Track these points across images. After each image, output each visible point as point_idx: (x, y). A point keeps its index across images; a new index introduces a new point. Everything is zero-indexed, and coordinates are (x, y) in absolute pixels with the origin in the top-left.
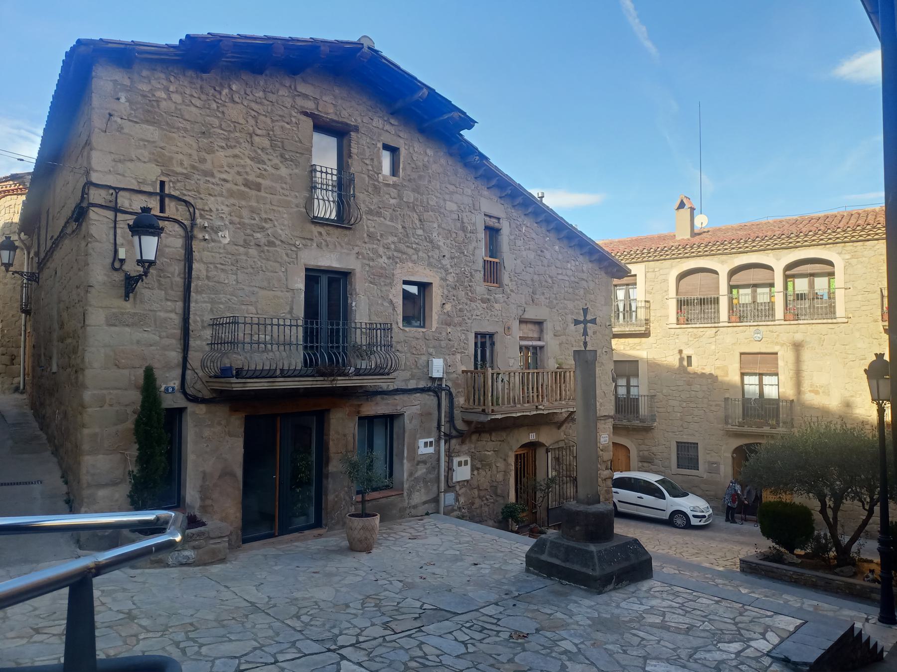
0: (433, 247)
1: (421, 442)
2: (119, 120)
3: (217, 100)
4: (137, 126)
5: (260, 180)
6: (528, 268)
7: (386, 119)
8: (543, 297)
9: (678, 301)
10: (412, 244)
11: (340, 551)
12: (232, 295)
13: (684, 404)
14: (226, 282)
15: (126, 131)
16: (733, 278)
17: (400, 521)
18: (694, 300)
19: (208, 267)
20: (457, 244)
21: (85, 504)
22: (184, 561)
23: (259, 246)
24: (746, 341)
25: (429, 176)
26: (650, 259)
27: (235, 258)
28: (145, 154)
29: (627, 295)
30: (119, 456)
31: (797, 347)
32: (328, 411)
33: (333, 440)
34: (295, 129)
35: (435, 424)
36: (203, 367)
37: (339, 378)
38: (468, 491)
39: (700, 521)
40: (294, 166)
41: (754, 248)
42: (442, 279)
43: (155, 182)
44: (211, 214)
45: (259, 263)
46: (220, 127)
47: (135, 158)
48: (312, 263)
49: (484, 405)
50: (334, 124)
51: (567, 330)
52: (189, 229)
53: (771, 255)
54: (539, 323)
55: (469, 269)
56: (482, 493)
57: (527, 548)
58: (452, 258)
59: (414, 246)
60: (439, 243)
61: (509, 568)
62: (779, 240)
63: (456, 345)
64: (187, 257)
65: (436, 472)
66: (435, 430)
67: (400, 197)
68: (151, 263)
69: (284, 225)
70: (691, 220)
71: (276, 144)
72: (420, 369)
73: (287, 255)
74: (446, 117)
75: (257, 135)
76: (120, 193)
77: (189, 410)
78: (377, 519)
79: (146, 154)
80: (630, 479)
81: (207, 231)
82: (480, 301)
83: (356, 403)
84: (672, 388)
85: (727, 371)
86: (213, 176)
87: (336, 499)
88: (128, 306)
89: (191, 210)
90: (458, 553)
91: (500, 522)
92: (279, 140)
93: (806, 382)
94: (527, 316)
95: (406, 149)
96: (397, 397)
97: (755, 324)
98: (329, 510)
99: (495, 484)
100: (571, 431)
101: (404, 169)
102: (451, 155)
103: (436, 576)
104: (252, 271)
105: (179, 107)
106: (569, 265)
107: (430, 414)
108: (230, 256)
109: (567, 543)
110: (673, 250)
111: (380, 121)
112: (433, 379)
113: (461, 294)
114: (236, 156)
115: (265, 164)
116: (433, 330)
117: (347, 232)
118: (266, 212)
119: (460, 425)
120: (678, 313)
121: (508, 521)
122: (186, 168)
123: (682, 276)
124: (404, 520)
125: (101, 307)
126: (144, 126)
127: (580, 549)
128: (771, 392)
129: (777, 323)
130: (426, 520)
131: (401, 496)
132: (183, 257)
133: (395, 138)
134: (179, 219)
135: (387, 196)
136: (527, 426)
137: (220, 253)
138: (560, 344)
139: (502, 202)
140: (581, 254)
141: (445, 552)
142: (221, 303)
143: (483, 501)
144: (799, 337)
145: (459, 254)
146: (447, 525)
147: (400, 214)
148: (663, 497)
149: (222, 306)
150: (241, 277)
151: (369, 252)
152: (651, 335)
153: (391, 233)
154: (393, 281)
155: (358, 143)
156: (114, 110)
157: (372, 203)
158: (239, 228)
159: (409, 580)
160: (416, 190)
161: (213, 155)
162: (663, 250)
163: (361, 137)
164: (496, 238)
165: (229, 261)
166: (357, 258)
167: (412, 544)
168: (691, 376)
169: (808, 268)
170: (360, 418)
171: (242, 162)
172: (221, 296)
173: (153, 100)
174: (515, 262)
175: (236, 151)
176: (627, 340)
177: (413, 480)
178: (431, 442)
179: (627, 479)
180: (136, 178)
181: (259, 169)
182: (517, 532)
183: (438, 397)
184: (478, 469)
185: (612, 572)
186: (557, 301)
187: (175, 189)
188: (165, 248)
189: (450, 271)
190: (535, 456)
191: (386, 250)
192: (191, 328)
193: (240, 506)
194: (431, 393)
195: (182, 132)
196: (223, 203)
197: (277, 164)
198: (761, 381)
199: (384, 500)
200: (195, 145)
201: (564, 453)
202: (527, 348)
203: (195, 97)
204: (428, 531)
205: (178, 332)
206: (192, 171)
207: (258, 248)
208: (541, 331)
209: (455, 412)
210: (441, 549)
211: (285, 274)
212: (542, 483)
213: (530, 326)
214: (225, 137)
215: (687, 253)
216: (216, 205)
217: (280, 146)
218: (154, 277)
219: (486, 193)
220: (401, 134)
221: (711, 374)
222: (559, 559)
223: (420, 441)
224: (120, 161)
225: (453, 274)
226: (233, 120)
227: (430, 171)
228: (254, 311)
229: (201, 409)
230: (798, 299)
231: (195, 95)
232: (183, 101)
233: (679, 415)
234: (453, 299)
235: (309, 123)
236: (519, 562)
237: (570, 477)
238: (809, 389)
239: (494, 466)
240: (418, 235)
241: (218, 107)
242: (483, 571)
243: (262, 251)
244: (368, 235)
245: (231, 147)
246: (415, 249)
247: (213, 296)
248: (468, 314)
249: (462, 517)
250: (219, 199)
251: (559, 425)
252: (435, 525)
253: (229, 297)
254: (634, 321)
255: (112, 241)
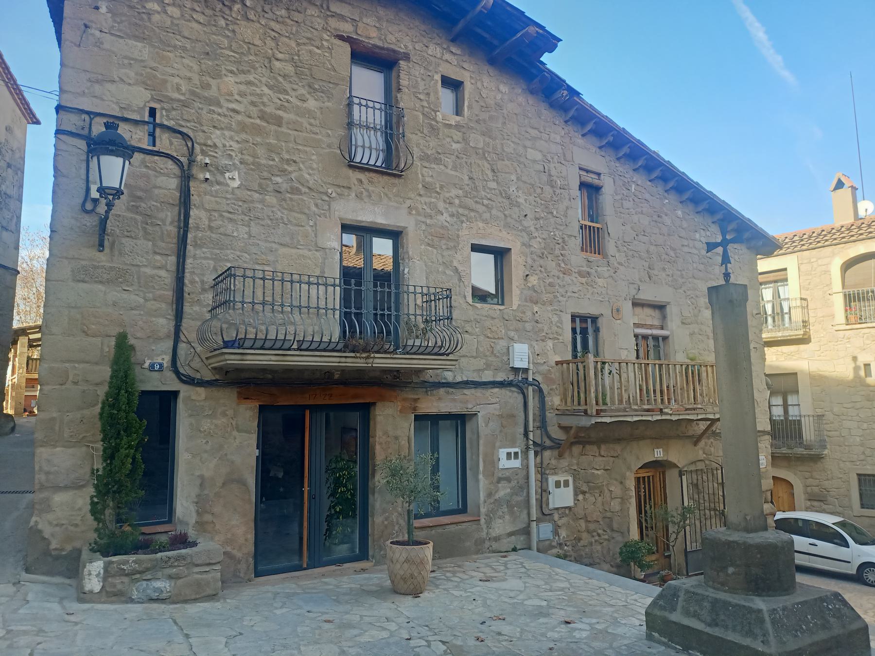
0: (510, 204)
1: (503, 453)
2: (97, 33)
3: (226, 17)
4: (121, 41)
5: (280, 113)
6: (640, 237)
7: (445, 46)
8: (664, 275)
9: (845, 295)
10: (482, 199)
11: (380, 593)
12: (242, 251)
13: (865, 426)
14: (235, 234)
15: (106, 46)
17: (476, 556)
19: (211, 215)
20: (543, 202)
21: (36, 512)
22: (155, 595)
25: (503, 117)
26: (804, 247)
27: (246, 206)
28: (131, 74)
29: (776, 294)
30: (84, 449)
32: (374, 404)
33: (381, 444)
34: (326, 54)
35: (521, 430)
36: (202, 340)
37: (377, 355)
38: (571, 522)
40: (326, 99)
42: (523, 244)
43: (143, 108)
44: (216, 150)
45: (279, 213)
46: (230, 48)
47: (117, 79)
48: (350, 217)
49: (586, 405)
50: (377, 50)
51: (699, 318)
52: (186, 168)
54: (661, 308)
55: (561, 234)
56: (592, 526)
57: (649, 600)
58: (537, 219)
59: (486, 202)
60: (519, 200)
61: (620, 631)
63: (546, 328)
64: (182, 200)
65: (525, 494)
66: (520, 437)
67: (465, 140)
68: (118, 193)
69: (313, 169)
70: (853, 202)
71: (302, 72)
73: (316, 205)
75: (277, 60)
76: (95, 119)
77: (181, 396)
78: (428, 551)
79: (132, 74)
80: (796, 520)
81: (209, 171)
82: (577, 275)
84: (845, 405)
86: (219, 105)
87: (386, 523)
88: (102, 258)
89: (190, 144)
90: (544, 603)
91: (618, 566)
92: (306, 66)
94: (643, 296)
95: (472, 84)
96: (466, 391)
98: (376, 537)
99: (608, 514)
100: (712, 449)
101: (470, 107)
102: (532, 92)
103: (501, 638)
104: (269, 222)
105: (176, 22)
106: (697, 236)
107: (512, 416)
108: (240, 203)
109: (714, 595)
110: (834, 234)
111: (438, 49)
112: (516, 370)
113: (551, 264)
114: (249, 83)
115: (288, 94)
116: (515, 307)
117: (396, 181)
118: (288, 152)
119: (556, 433)
120: (846, 310)
121: (629, 565)
122: (183, 94)
123: (848, 265)
124: (480, 556)
125: (67, 258)
126: (131, 42)
127: (737, 605)
130: (512, 556)
131: (476, 522)
132: (178, 202)
133: (458, 70)
134: (175, 154)
135: (448, 140)
136: (650, 438)
137: (227, 199)
138: (692, 334)
139: (603, 153)
140: (713, 222)
141: (525, 602)
143: (593, 536)
145: (546, 214)
146: (539, 565)
147: (466, 163)
148: (847, 545)
150: (255, 229)
151: (425, 207)
152: (812, 340)
153: (455, 184)
154: (459, 244)
155: (409, 74)
156: (92, 21)
157: (428, 147)
158: (252, 169)
159: (459, 642)
160: (487, 133)
161: (219, 80)
162: (820, 235)
163: (413, 66)
164: (596, 198)
165: (240, 209)
166: (410, 213)
167: (481, 587)
170: (418, 418)
171: (258, 91)
173: (144, 13)
174: (623, 228)
175: (251, 78)
176: (780, 348)
177: (494, 503)
178: (516, 454)
179: (792, 521)
180: (117, 103)
182: (643, 581)
183: (523, 394)
184: (584, 493)
185: (799, 649)
186: (683, 280)
187: (169, 119)
188: (153, 189)
189: (534, 235)
190: (664, 481)
191: (447, 206)
192: (186, 289)
193: (252, 525)
194: (514, 389)
195: (180, 51)
196: (231, 138)
197: (304, 95)
199: (452, 528)
200: (196, 68)
201: (705, 478)
202: (645, 337)
203: (197, 11)
204: (509, 572)
205: (169, 294)
206: (192, 98)
207: (279, 195)
208: (664, 317)
209: (548, 414)
210: (521, 597)
211: (314, 229)
212: (675, 514)
213: (648, 311)
214: (235, 60)
215: (852, 236)
216: (223, 140)
217: (308, 74)
218: (139, 224)
219: (580, 141)
220: (466, 65)
222: (702, 621)
223: (501, 450)
224: (97, 81)
225: (538, 239)
226: (246, 40)
227: (505, 111)
229: (201, 393)
231: (198, 9)
232: (183, 16)
233: (858, 439)
234: (540, 271)
235: (347, 49)
236: (637, 623)
237: (715, 510)
239: (606, 491)
240: (491, 189)
241: (227, 25)
242: (577, 634)
244: (423, 186)
245: (243, 72)
246: (487, 206)
248: (561, 290)
249: (565, 557)
250: (227, 133)
251: (696, 440)
252: (522, 563)
254: (787, 325)
255: (84, 177)
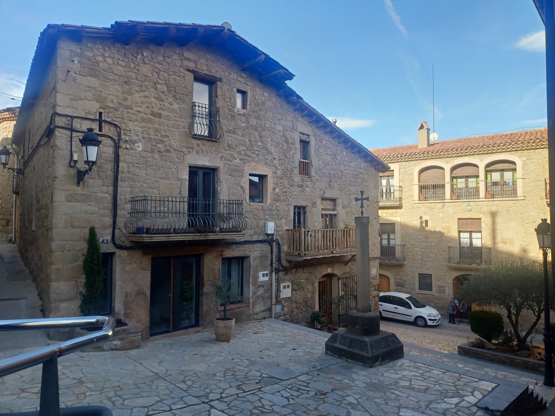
0: (268, 153)
1: (261, 274)
2: (74, 74)
3: (134, 62)
4: (85, 78)
5: (161, 112)
6: (327, 166)
7: (239, 73)
8: (336, 184)
9: (419, 186)
10: (255, 151)
11: (211, 341)
12: (144, 182)
13: (423, 250)
14: (140, 174)
15: (78, 81)
16: (453, 172)
17: (248, 322)
18: (429, 185)
19: (129, 165)
20: (283, 151)
21: (52, 312)
22: (114, 347)
23: (160, 152)
24: (462, 211)
25: (266, 109)
26: (402, 160)
27: (145, 160)
28: (90, 95)
29: (388, 183)
30: (74, 282)
31: (493, 215)
32: (203, 254)
33: (206, 273)
34: (182, 80)
35: (269, 263)
36: (126, 227)
37: (210, 234)
38: (290, 304)
39: (433, 323)
40: (182, 103)
41: (467, 154)
42: (273, 173)
43: (96, 113)
44: (131, 133)
45: (160, 163)
46: (136, 79)
47: (84, 98)
48: (193, 163)
49: (300, 251)
50: (207, 77)
51: (351, 205)
52: (117, 142)
53: (477, 158)
54: (334, 200)
55: (290, 166)
56: (298, 305)
57: (326, 339)
58: (280, 160)
59: (256, 152)
60: (271, 151)
61: (315, 351)
62: (482, 148)
63: (282, 214)
64: (116, 159)
65: (270, 292)
66: (269, 266)
67: (248, 122)
68: (94, 163)
69: (176, 140)
70: (427, 136)
71: (171, 89)
72: (260, 228)
73: (178, 158)
74: (276, 72)
75: (159, 84)
76: (74, 119)
77: (117, 254)
78: (233, 321)
79: (90, 95)
80: (390, 296)
81: (128, 143)
82: (297, 187)
83: (220, 249)
84: (416, 240)
85: (450, 230)
86: (132, 109)
87: (208, 309)
88: (79, 189)
89: (118, 130)
90: (283, 342)
91: (309, 323)
92: (173, 86)
93: (499, 236)
94: (326, 196)
95: (251, 92)
96: (246, 246)
97: (467, 200)
98: (203, 316)
99: (306, 300)
100: (353, 267)
101: (250, 105)
102: (279, 96)
103: (270, 357)
104: (156, 168)
105: (111, 66)
106: (352, 164)
107: (266, 256)
108: (142, 159)
109: (351, 336)
110: (417, 155)
111: (235, 75)
112: (268, 235)
113: (286, 182)
114: (146, 97)
115: (164, 101)
116: (268, 204)
117: (215, 144)
118: (164, 131)
119: (285, 263)
120: (419, 194)
121: (314, 323)
122: (115, 104)
123: (422, 171)
124: (250, 322)
125: (63, 190)
126: (89, 78)
127: (359, 340)
128: (477, 243)
129: (481, 200)
130: (264, 322)
131: (248, 307)
132: (113, 159)
133: (244, 85)
134: (111, 135)
135: (240, 121)
136: (326, 263)
137: (136, 157)
138: (347, 213)
139: (311, 125)
140: (360, 157)
141: (275, 342)
142: (137, 188)
143: (299, 310)
144: (494, 209)
145: (284, 157)
146: (277, 325)
147: (248, 133)
148: (410, 308)
149: (137, 190)
150: (149, 171)
151: (228, 156)
152: (403, 207)
153: (242, 144)
154: (243, 174)
155: (221, 89)
156: (71, 68)
157: (230, 126)
158: (148, 141)
159: (253, 359)
160: (258, 118)
161: (132, 96)
162: (410, 155)
163: (224, 85)
164: (307, 147)
165: (142, 161)
166: (221, 159)
167: (255, 337)
168: (428, 233)
169: (500, 166)
170: (223, 259)
171: (150, 100)
172: (137, 183)
173: (95, 62)
174: (319, 162)
175: (146, 94)
176: (388, 210)
177: (256, 297)
178: (267, 274)
179: (388, 297)
180: (84, 110)
181: (160, 105)
182: (320, 330)
183: (271, 245)
184: (296, 290)
186: (345, 187)
187: (108, 117)
188: (102, 154)
189: (278, 168)
190: (331, 282)
191: (239, 155)
192: (118, 203)
193: (149, 313)
194: (267, 243)
195: (113, 82)
196: (138, 126)
197: (172, 102)
198: (471, 236)
199: (237, 310)
200: (121, 90)
201: (349, 280)
202: (326, 215)
203: (121, 60)
204: (265, 329)
205: (110, 205)
206: (119, 106)
207: (160, 153)
208: (335, 205)
209: (282, 255)
210: (273, 340)
211: (176, 170)
212: (336, 299)
213: (328, 202)
214: (139, 85)
215: (425, 157)
216: (134, 127)
217: (173, 90)
218: (96, 171)
219: (301, 119)
220: (248, 83)
221: (440, 232)
222: (346, 346)
223: (260, 273)
224: (74, 100)
225: (280, 170)
226: (144, 74)
227: (266, 106)
228: (157, 193)
229: (124, 253)
230: (494, 185)
231: (121, 59)
232: (113, 63)
233: (420, 257)
234: (281, 185)
235: (191, 76)
236: (321, 348)
237: (353, 295)
238: (501, 241)
239: (306, 289)
240: (259, 146)
241: (135, 66)
242: (299, 354)
243: (162, 156)
244: (227, 146)
245: (143, 91)
246: (257, 154)
247: (132, 183)
248: (289, 194)
249: (286, 320)
250: (136, 123)
251: (346, 263)
252: (269, 325)
253: (141, 184)
254: (392, 199)
255: (69, 149)
